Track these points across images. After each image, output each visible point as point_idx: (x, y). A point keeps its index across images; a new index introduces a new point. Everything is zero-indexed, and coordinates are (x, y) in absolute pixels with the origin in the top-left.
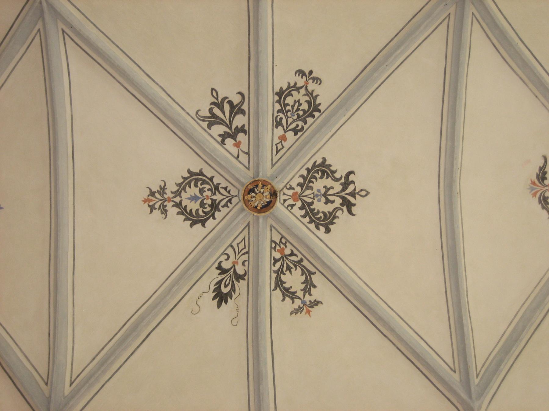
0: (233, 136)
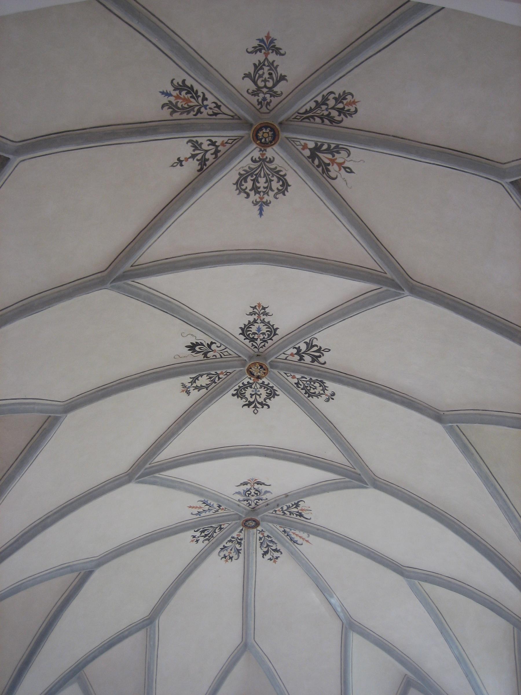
0: (298, 353)
